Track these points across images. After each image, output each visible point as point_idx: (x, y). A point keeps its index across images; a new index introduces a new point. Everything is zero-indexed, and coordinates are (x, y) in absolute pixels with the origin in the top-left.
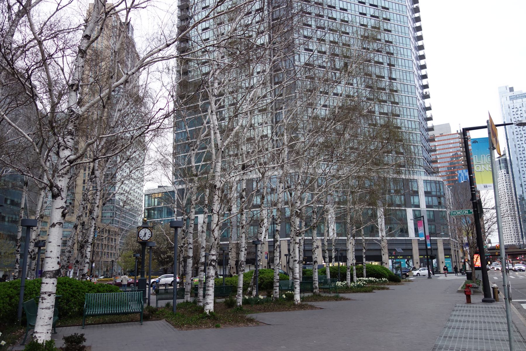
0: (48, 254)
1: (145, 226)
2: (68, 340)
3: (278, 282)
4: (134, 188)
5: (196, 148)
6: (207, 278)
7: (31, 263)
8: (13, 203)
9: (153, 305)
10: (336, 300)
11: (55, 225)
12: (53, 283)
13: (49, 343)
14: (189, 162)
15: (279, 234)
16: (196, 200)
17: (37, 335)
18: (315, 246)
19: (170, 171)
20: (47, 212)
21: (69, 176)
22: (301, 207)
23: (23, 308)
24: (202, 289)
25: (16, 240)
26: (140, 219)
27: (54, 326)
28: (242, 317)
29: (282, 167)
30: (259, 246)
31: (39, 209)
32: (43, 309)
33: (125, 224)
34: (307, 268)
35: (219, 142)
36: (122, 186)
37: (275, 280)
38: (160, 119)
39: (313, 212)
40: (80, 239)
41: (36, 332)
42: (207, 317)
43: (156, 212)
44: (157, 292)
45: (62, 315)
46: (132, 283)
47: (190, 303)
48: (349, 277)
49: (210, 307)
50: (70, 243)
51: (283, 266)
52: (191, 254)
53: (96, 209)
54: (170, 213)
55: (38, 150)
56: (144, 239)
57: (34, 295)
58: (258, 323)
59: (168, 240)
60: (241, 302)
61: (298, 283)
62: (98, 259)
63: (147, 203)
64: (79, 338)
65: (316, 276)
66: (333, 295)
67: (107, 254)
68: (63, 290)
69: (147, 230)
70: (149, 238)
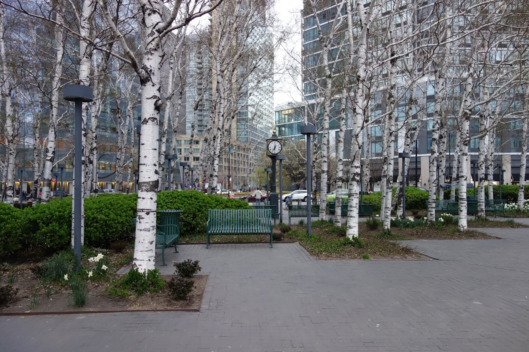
3: (434, 202)
6: (350, 195)
9: (286, 222)
11: (147, 122)
12: (151, 199)
13: (153, 274)
15: (436, 143)
16: (330, 106)
17: (137, 263)
22: (472, 107)
24: (340, 208)
32: (141, 230)
37: (430, 200)
41: (136, 259)
42: (350, 243)
43: (287, 129)
44: (290, 208)
47: (326, 221)
49: (353, 232)
51: (423, 184)
52: (325, 168)
56: (273, 153)
58: (419, 255)
59: (299, 156)
60: (389, 226)
61: (466, 204)
64: (191, 267)
68: (190, 204)
69: (276, 142)
70: (279, 151)
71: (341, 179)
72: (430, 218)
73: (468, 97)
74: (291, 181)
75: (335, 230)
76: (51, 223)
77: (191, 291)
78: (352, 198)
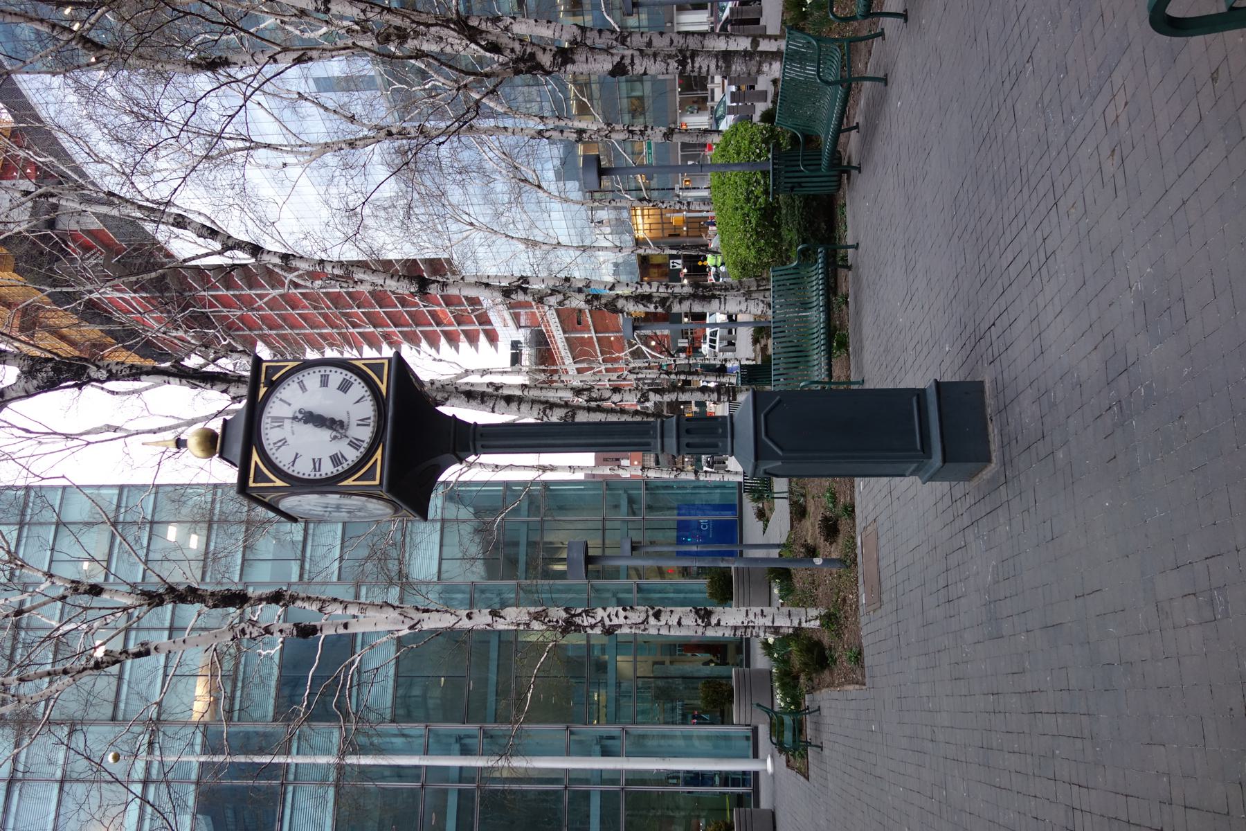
56: (366, 434)
70: (359, 389)
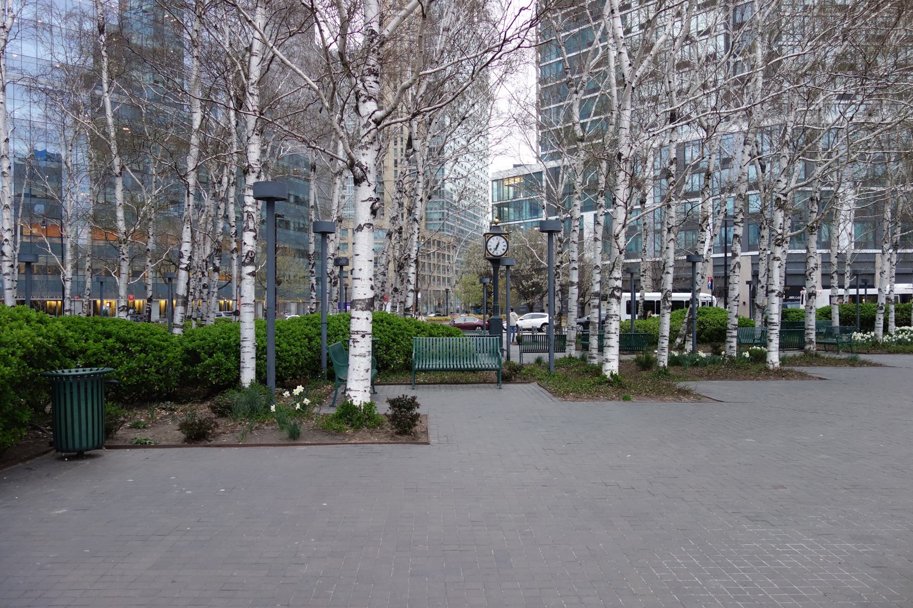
0: (357, 274)
1: (495, 231)
2: (393, 403)
3: (736, 329)
4: (474, 169)
5: (581, 89)
7: (331, 291)
8: (298, 201)
9: (515, 359)
10: (853, 365)
13: (370, 406)
14: (569, 117)
17: (352, 394)
18: (813, 266)
19: (533, 135)
20: (345, 213)
21: (376, 146)
23: (328, 354)
24: (596, 337)
25: (308, 256)
26: (487, 220)
27: (373, 384)
28: (668, 386)
29: (749, 113)
30: (699, 265)
31: (335, 207)
33: (462, 231)
34: (789, 306)
35: (627, 70)
36: (455, 167)
37: (729, 326)
38: (521, 31)
39: (812, 199)
40: (397, 254)
41: (350, 390)
43: (512, 210)
45: (383, 368)
46: (479, 326)
47: (575, 359)
48: (880, 323)
49: (612, 367)
50: (383, 261)
52: (575, 279)
53: (419, 204)
54: (535, 210)
55: (327, 104)
57: (342, 335)
58: (699, 397)
59: (532, 257)
61: (777, 331)
62: (425, 287)
63: (496, 194)
65: (812, 321)
66: (844, 356)
67: (439, 280)
68: (380, 331)
71: (597, 295)
72: (729, 352)
73: (783, 176)
74: (519, 297)
75: (589, 369)
76: (214, 352)
77: (415, 425)
78: (610, 321)
